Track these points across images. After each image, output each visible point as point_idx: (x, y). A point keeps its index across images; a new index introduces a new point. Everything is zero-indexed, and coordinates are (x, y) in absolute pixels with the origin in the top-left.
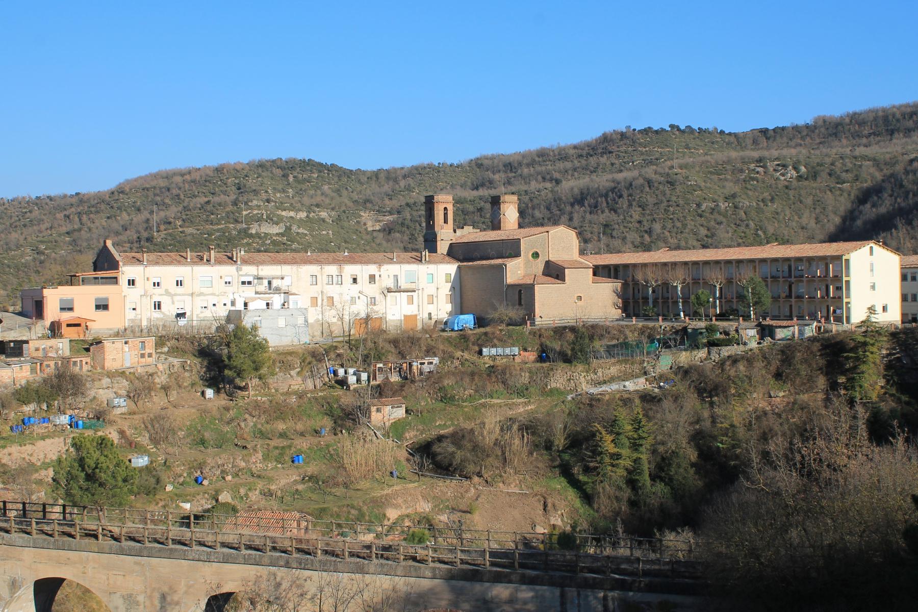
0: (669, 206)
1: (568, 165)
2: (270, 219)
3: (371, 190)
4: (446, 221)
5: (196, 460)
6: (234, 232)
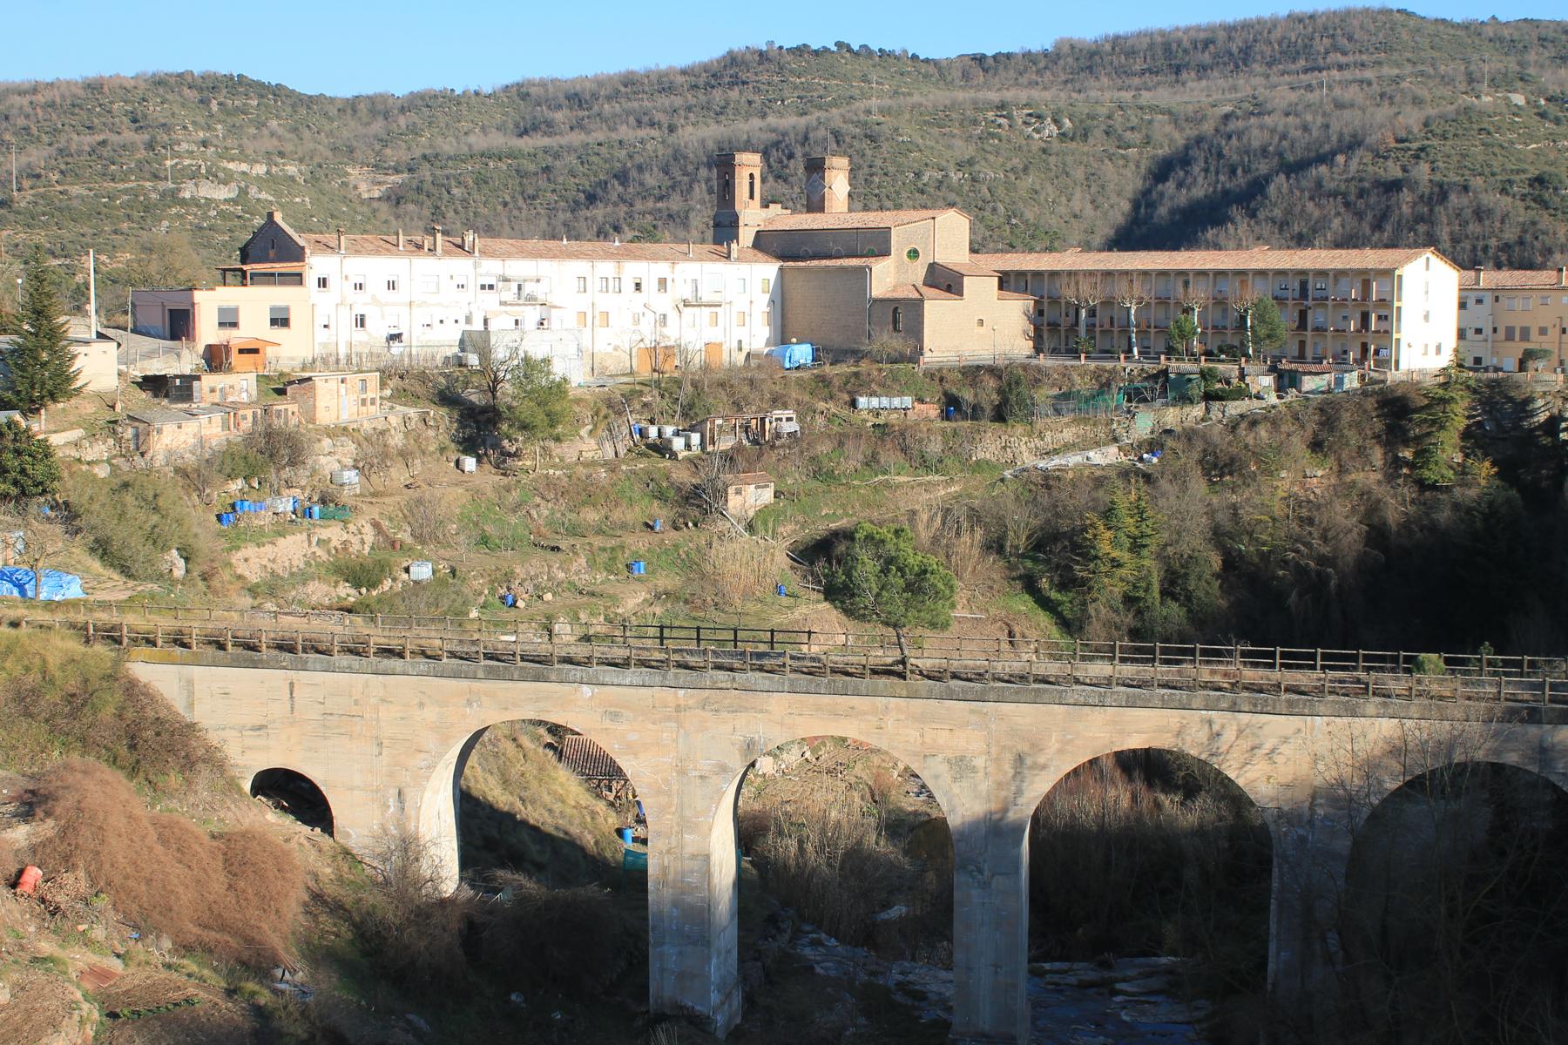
0: (872, 175)
1: (678, 101)
2: (212, 175)
3: (349, 130)
4: (752, 197)
5: (498, 569)
6: (154, 196)
